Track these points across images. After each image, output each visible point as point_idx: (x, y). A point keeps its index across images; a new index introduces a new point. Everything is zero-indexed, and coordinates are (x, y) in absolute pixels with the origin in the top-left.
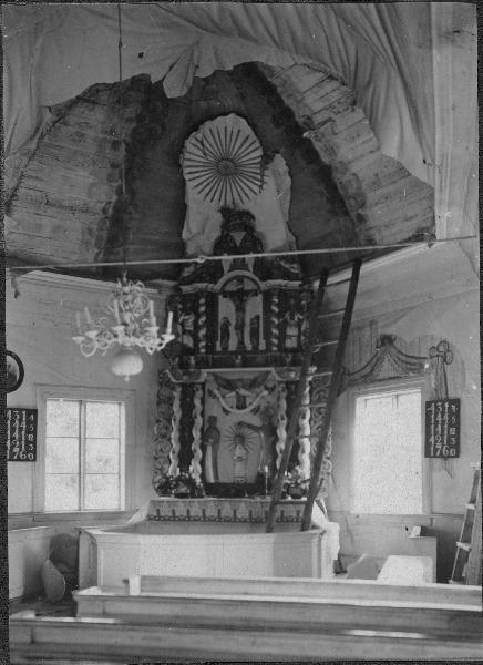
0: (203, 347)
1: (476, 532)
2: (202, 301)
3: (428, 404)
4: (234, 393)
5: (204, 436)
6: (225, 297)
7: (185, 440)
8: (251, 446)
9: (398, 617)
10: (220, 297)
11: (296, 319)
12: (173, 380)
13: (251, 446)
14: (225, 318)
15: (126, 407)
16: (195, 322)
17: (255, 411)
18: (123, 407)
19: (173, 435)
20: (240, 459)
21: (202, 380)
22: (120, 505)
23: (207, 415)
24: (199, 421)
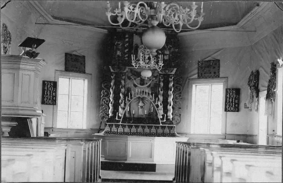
0: (127, 57)
1: (226, 179)
2: (127, 36)
3: (227, 90)
4: (139, 78)
5: (125, 95)
6: (136, 35)
7: (117, 98)
8: (146, 101)
9: (213, 49)
10: (134, 34)
11: (169, 47)
12: (112, 71)
13: (146, 101)
14: (136, 44)
15: (88, 82)
16: (123, 45)
17: (148, 87)
18: (86, 81)
19: (111, 96)
20: (142, 107)
21: (125, 71)
22: (15, 81)
23: (127, 86)
24: (123, 90)
